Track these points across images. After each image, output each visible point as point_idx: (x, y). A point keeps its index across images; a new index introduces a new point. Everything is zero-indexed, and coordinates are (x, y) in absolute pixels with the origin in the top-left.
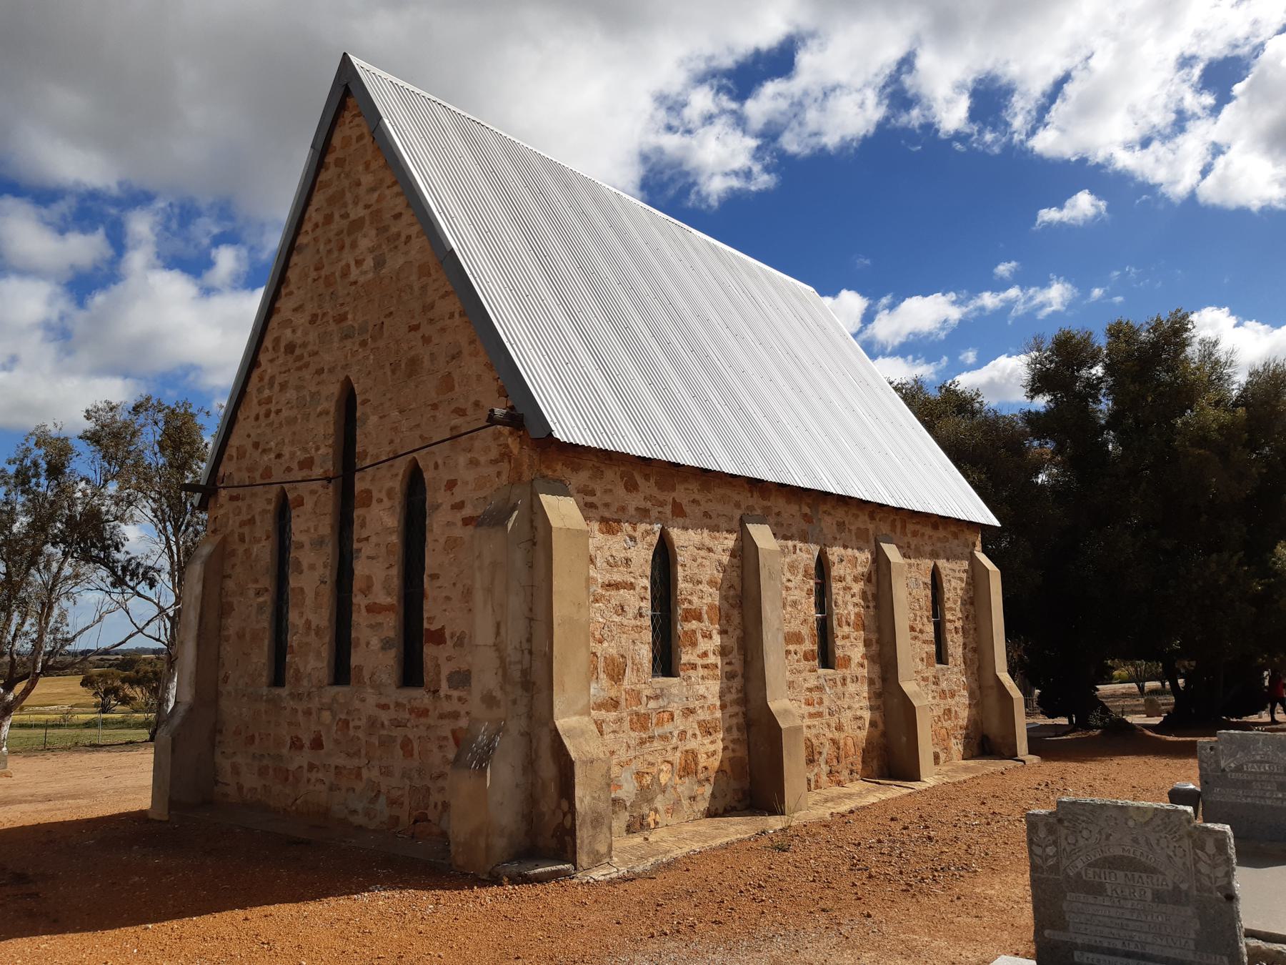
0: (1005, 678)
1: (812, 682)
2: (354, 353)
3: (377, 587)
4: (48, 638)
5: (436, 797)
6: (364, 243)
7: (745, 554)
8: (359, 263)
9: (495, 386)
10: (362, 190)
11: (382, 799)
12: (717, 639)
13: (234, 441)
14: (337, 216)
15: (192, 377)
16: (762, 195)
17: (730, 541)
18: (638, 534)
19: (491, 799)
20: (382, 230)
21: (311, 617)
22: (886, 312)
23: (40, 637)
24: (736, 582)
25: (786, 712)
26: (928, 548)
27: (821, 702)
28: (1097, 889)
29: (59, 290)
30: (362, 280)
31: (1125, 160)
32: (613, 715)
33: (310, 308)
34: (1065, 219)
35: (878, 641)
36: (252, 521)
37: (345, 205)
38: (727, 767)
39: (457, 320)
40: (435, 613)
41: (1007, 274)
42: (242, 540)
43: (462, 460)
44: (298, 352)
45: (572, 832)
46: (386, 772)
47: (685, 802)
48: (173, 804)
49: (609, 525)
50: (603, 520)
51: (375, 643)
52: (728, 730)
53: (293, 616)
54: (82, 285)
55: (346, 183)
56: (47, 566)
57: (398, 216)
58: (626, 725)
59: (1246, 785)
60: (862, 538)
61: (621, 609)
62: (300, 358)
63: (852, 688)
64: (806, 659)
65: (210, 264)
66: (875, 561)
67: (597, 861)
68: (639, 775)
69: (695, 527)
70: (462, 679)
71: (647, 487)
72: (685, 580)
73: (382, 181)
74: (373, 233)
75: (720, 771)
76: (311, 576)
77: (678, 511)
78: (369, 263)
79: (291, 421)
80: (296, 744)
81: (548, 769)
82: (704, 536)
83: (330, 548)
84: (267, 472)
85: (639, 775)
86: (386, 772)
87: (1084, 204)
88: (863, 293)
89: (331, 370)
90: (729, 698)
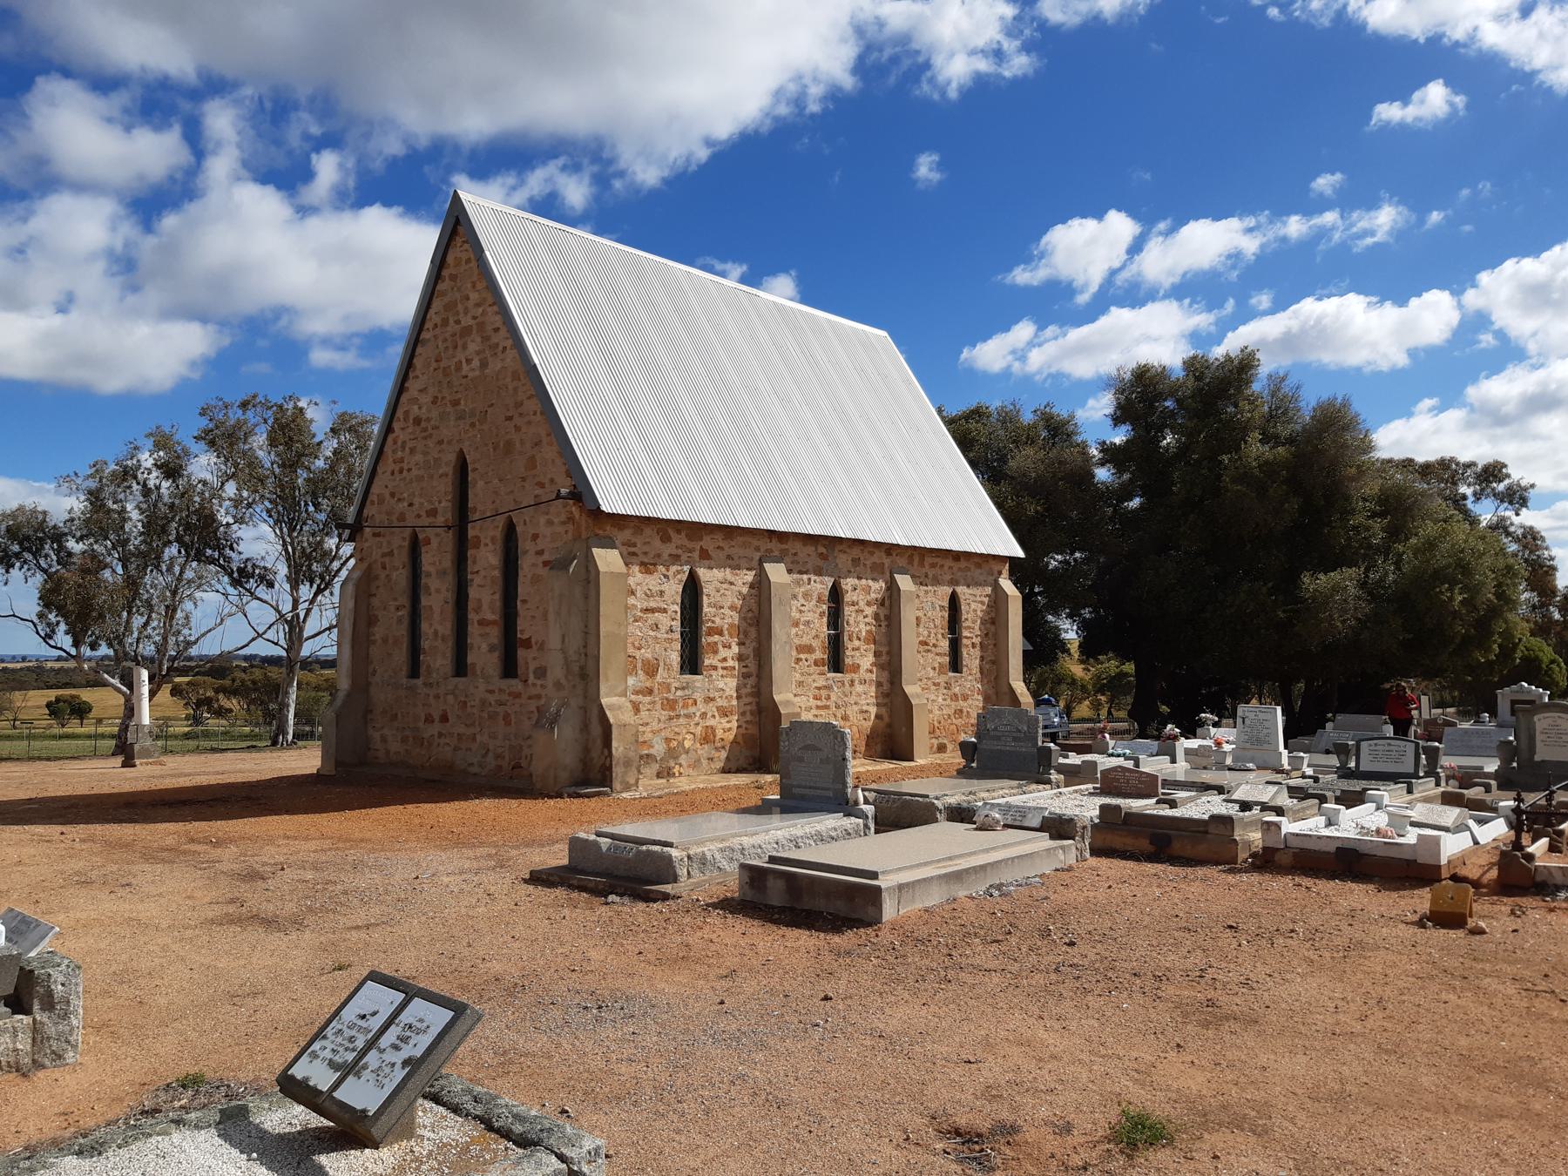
0: (1019, 687)
1: (821, 682)
2: (466, 432)
3: (485, 607)
4: (172, 640)
5: (526, 751)
6: (473, 347)
7: (761, 586)
8: (468, 361)
9: (563, 469)
10: (470, 304)
11: (490, 754)
12: (735, 649)
13: (375, 490)
14: (451, 321)
15: (283, 322)
16: (1018, 83)
17: (749, 576)
18: (670, 574)
19: (560, 746)
20: (486, 339)
21: (439, 628)
22: (1161, 239)
23: (165, 639)
24: (754, 607)
25: (788, 703)
26: (948, 577)
27: (828, 698)
28: (801, 760)
29: (121, 211)
30: (471, 375)
31: (1493, 36)
32: (648, 699)
33: (432, 391)
34: (1409, 120)
35: (888, 653)
36: (391, 554)
37: (457, 313)
38: (740, 739)
39: (538, 417)
40: (524, 628)
41: (1329, 192)
42: (384, 568)
43: (543, 520)
44: (423, 424)
45: (610, 768)
46: (493, 736)
47: (705, 762)
48: (338, 764)
49: (647, 568)
50: (642, 564)
51: (484, 647)
52: (743, 714)
53: (424, 626)
54: (151, 203)
55: (458, 295)
56: (170, 569)
57: (497, 330)
58: (658, 706)
59: (998, 738)
60: (876, 571)
61: (656, 627)
62: (425, 430)
63: (859, 688)
64: (816, 664)
65: (308, 175)
66: (888, 589)
67: (627, 788)
68: (668, 740)
69: (719, 567)
70: (541, 672)
71: (679, 539)
72: (710, 605)
73: (485, 299)
74: (479, 339)
75: (734, 742)
76: (438, 598)
77: (705, 555)
78: (476, 363)
79: (420, 479)
80: (429, 719)
81: (596, 730)
82: (728, 574)
83: (450, 579)
84: (402, 517)
85: (668, 740)
86: (493, 736)
87: (1435, 98)
88: (1133, 214)
89: (449, 442)
90: (744, 691)
